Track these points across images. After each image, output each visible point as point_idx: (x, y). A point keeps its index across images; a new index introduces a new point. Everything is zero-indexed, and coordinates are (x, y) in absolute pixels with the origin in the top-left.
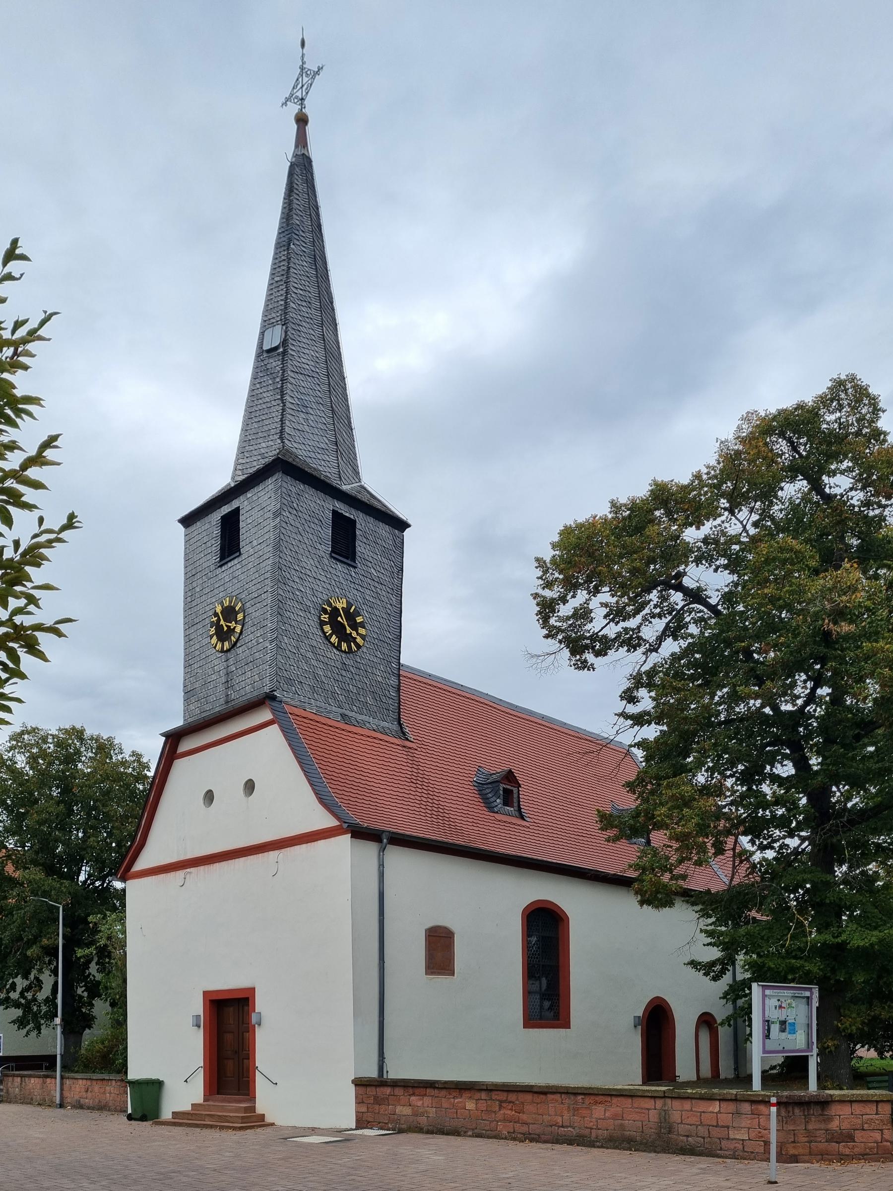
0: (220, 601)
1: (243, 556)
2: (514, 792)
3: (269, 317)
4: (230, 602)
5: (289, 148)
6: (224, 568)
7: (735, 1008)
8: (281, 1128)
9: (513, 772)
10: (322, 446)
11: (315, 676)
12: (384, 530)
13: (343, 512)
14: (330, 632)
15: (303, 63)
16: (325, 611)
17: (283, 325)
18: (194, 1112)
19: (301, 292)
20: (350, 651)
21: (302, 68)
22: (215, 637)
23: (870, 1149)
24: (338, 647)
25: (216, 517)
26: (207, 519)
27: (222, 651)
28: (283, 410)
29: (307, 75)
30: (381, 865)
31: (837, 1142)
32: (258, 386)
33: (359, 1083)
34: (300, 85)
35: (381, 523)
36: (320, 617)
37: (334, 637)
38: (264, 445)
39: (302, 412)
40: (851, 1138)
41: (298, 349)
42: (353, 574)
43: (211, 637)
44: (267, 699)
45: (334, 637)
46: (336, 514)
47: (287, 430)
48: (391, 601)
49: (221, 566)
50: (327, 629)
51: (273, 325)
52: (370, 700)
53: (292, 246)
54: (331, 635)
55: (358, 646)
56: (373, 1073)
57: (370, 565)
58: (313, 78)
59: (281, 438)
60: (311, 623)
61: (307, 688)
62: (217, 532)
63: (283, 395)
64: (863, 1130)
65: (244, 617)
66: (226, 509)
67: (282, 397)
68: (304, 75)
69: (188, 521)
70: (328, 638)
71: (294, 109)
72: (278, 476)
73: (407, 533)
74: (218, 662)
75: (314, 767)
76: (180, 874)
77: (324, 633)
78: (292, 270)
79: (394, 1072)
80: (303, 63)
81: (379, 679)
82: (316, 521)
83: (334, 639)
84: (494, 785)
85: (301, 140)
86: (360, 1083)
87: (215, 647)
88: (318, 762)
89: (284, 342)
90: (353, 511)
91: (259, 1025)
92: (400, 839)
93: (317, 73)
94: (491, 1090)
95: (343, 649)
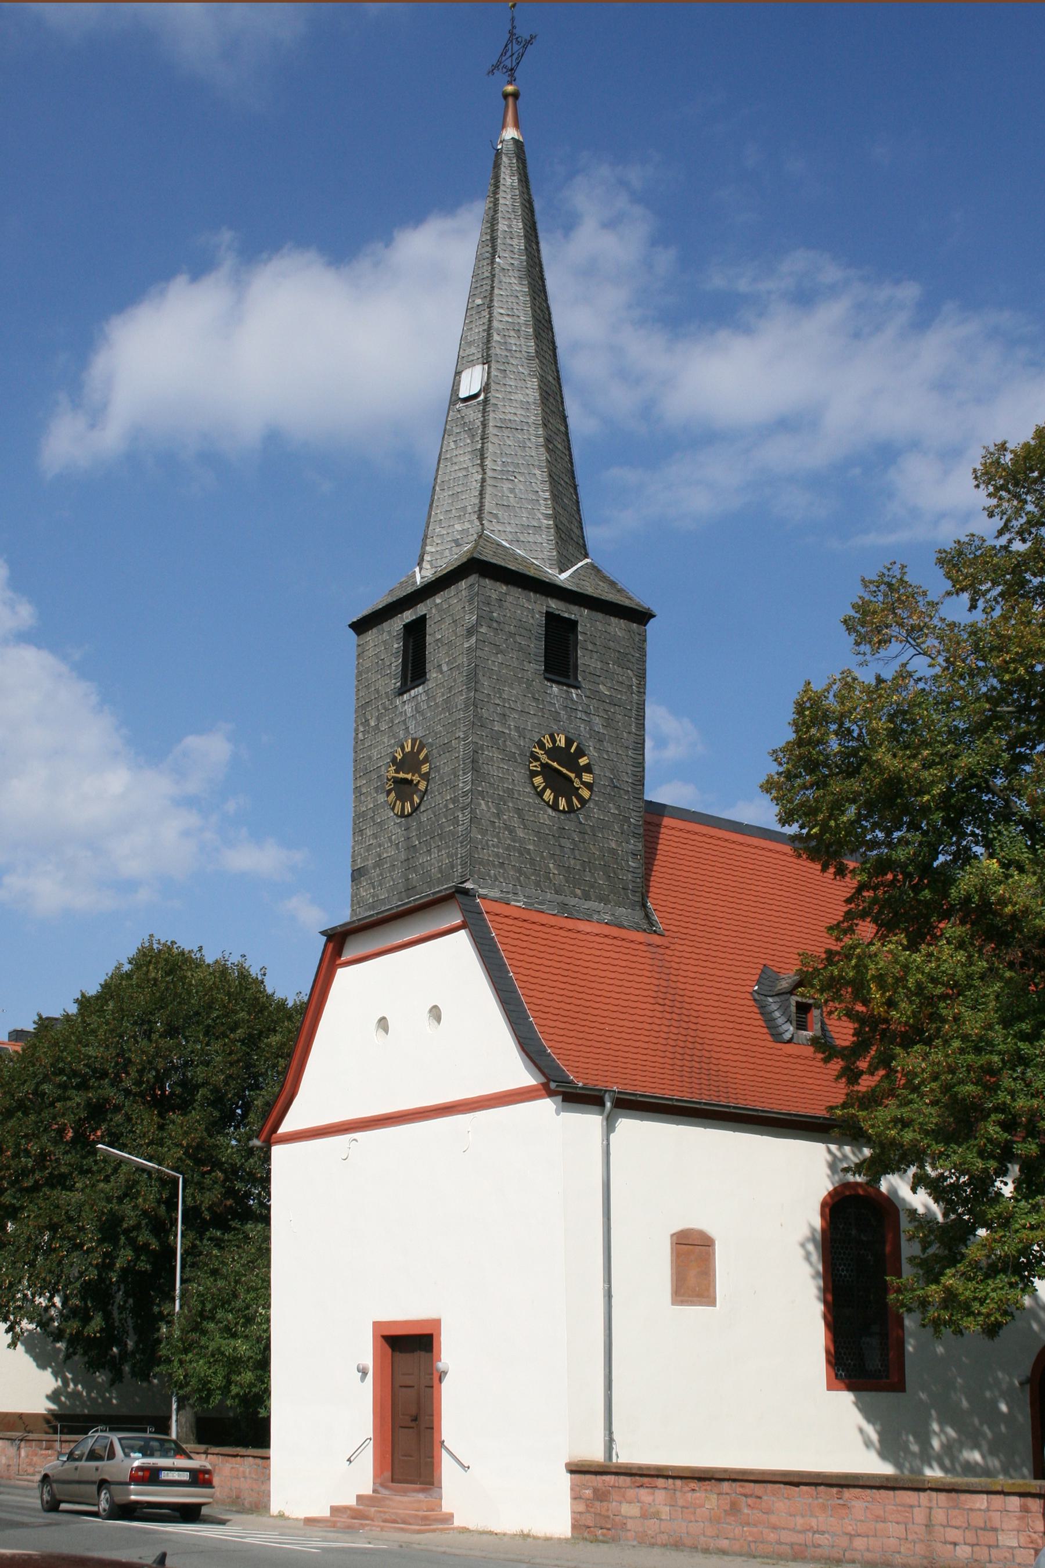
0: (400, 744)
3: (467, 352)
6: (406, 697)
7: (985, 1563)
11: (522, 851)
12: (617, 627)
13: (560, 612)
15: (514, 27)
17: (484, 364)
21: (511, 33)
24: (555, 807)
26: (385, 625)
27: (402, 816)
28: (483, 480)
29: (518, 43)
33: (574, 1468)
34: (509, 54)
35: (612, 618)
37: (548, 791)
44: (459, 895)
45: (548, 791)
46: (550, 616)
51: (472, 364)
53: (498, 260)
54: (544, 790)
55: (583, 801)
56: (596, 1454)
58: (525, 47)
59: (480, 518)
62: (397, 645)
63: (483, 458)
66: (408, 616)
67: (482, 462)
68: (514, 41)
69: (361, 626)
72: (473, 578)
73: (652, 625)
74: (395, 829)
78: (496, 291)
79: (626, 1455)
80: (514, 27)
83: (548, 795)
84: (783, 997)
87: (393, 809)
88: (523, 985)
89: (486, 388)
90: (575, 609)
93: (529, 42)
95: (561, 808)
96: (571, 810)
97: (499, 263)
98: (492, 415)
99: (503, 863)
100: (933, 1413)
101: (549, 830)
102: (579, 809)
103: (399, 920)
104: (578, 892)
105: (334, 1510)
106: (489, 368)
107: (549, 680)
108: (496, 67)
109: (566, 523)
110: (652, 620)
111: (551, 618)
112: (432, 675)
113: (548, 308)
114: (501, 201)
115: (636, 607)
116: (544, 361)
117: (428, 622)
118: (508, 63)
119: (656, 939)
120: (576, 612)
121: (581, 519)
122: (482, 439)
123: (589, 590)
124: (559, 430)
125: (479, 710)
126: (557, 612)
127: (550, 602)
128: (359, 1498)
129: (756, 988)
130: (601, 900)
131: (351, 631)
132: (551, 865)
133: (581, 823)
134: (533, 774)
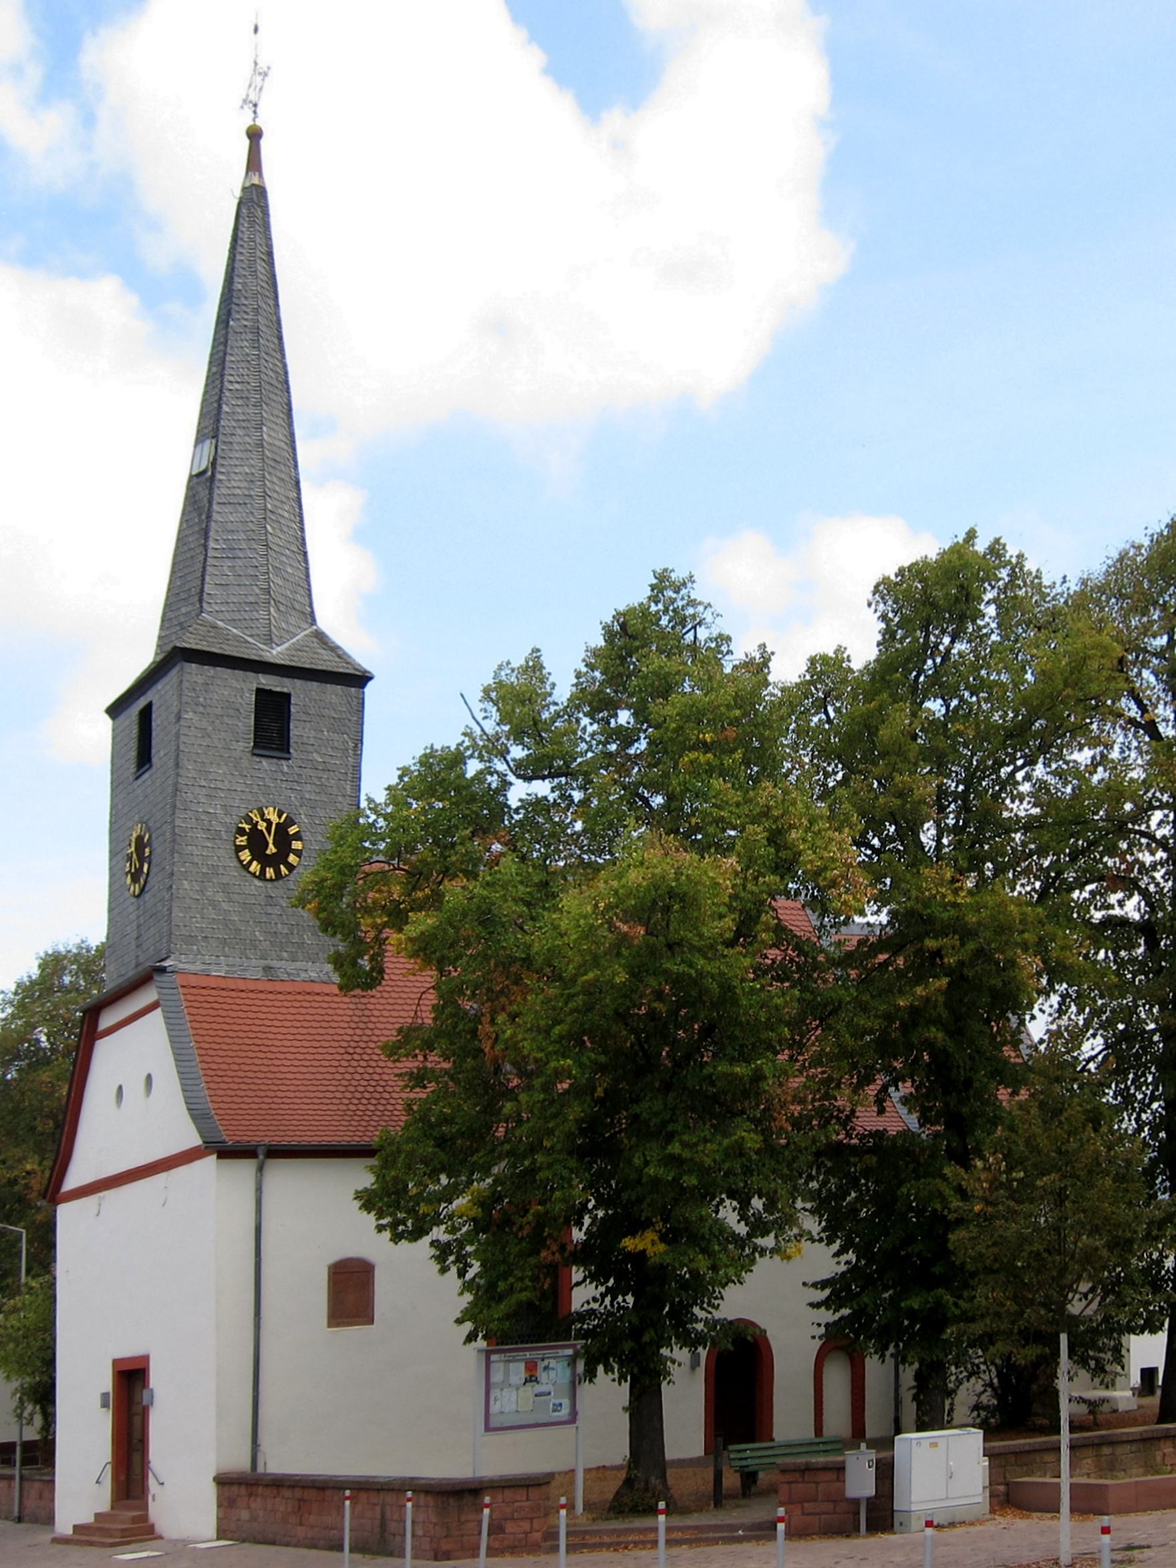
6: (139, 781)
8: (170, 1541)
10: (252, 599)
12: (334, 693)
14: (249, 858)
16: (241, 832)
18: (99, 1525)
19: (237, 386)
24: (262, 876)
27: (134, 896)
30: (259, 1190)
36: (235, 842)
37: (255, 863)
39: (229, 558)
42: (285, 769)
45: (255, 863)
46: (260, 692)
47: (207, 588)
49: (137, 778)
50: (246, 855)
53: (231, 323)
54: (250, 863)
55: (291, 868)
57: (310, 748)
63: (206, 538)
65: (151, 852)
66: (142, 703)
69: (114, 711)
73: (369, 688)
77: (241, 862)
82: (231, 712)
83: (255, 867)
85: (254, 162)
86: (223, 1481)
89: (214, 463)
90: (286, 681)
91: (152, 1404)
92: (283, 1151)
95: (268, 876)
97: (232, 327)
99: (206, 937)
100: (846, 1311)
101: (256, 899)
102: (286, 875)
103: (119, 1002)
106: (217, 441)
111: (262, 695)
115: (352, 671)
116: (274, 426)
117: (154, 708)
126: (268, 688)
128: (97, 1515)
132: (257, 933)
134: (239, 849)
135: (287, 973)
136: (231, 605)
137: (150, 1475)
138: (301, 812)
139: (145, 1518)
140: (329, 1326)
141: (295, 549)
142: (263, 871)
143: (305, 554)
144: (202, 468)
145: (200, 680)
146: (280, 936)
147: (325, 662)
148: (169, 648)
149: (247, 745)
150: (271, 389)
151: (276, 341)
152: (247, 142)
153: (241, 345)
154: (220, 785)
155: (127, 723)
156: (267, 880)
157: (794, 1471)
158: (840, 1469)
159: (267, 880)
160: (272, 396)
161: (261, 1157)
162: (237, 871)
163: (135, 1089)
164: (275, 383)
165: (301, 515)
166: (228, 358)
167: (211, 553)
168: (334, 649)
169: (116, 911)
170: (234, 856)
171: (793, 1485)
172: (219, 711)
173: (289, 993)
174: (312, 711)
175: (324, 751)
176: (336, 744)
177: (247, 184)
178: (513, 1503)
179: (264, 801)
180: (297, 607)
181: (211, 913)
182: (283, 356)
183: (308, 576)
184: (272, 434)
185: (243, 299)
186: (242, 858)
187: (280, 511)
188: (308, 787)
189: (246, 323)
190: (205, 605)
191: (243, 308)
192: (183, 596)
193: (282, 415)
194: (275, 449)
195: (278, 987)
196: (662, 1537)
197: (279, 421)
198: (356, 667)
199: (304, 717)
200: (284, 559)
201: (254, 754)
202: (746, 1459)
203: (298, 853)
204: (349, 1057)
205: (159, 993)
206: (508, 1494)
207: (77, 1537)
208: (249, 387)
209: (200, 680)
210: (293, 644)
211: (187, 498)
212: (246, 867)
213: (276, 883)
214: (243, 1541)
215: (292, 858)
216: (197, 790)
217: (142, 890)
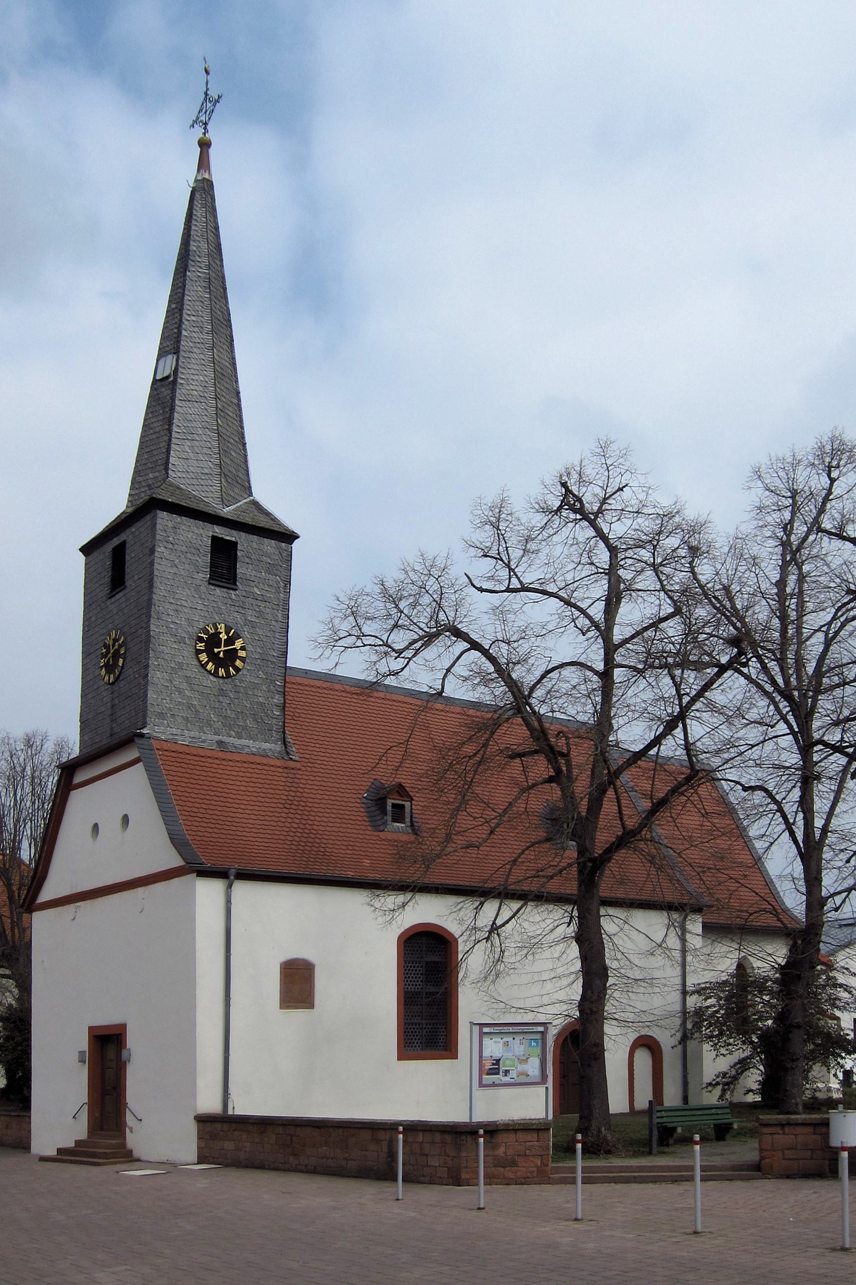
1: (127, 590)
2: (406, 806)
3: (165, 345)
4: (116, 635)
5: (189, 174)
6: (113, 600)
9: (403, 787)
10: (207, 471)
11: (190, 706)
12: (269, 546)
13: (223, 536)
14: (206, 659)
15: (207, 89)
16: (201, 639)
19: (193, 318)
20: (228, 675)
21: (206, 94)
22: (104, 669)
23: (531, 1172)
24: (215, 674)
25: (109, 547)
27: (109, 684)
30: (228, 902)
31: (503, 1167)
32: (150, 416)
36: (196, 647)
38: (151, 476)
40: (513, 1163)
41: (187, 376)
42: (234, 597)
43: (102, 667)
45: (210, 664)
46: (215, 539)
47: (172, 460)
48: (276, 618)
50: (204, 657)
52: (250, 723)
53: (188, 273)
54: (207, 663)
55: (238, 670)
60: (185, 653)
61: (180, 720)
64: (526, 1155)
65: (126, 651)
66: (116, 542)
69: (87, 550)
70: (204, 666)
71: (198, 132)
73: (296, 544)
75: (171, 805)
76: (70, 909)
77: (200, 662)
80: (207, 89)
81: (261, 700)
82: (194, 551)
83: (210, 666)
85: (204, 163)
89: (176, 371)
90: (234, 532)
91: (129, 1061)
93: (217, 101)
94: (285, 1125)
95: (220, 674)
96: (228, 675)
98: (178, 391)
101: (211, 691)
104: (233, 733)
105: (60, 1151)
107: (213, 585)
108: (195, 122)
109: (234, 471)
110: (296, 541)
112: (129, 583)
113: (228, 309)
114: (193, 228)
115: (284, 531)
116: (222, 351)
117: (127, 545)
118: (203, 118)
119: (292, 764)
120: (236, 535)
121: (248, 468)
122: (170, 410)
123: (247, 519)
124: (232, 402)
125: (157, 608)
126: (220, 536)
127: (216, 529)
129: (365, 795)
130: (251, 738)
131: (81, 553)
132: (212, 716)
133: (236, 686)
134: (198, 652)
135: (235, 747)
136: (191, 474)
137: (128, 1112)
138: (245, 629)
139: (124, 1145)
140: (280, 1008)
141: (237, 440)
142: (216, 670)
143: (244, 444)
144: (166, 374)
145: (170, 524)
146: (229, 719)
147: (263, 522)
148: (145, 498)
149: (204, 576)
150: (219, 323)
151: (222, 291)
152: (198, 150)
153: (195, 291)
154: (184, 603)
155: (102, 557)
156: (220, 677)
157: (776, 1125)
158: (826, 1124)
159: (220, 677)
160: (219, 328)
161: (232, 878)
162: (197, 668)
163: (110, 826)
164: (222, 320)
165: (241, 416)
166: (186, 298)
167: (174, 435)
168: (268, 514)
169: (90, 696)
170: (195, 657)
171: (774, 1136)
172: (184, 549)
173: (238, 761)
174: (253, 557)
175: (262, 586)
176: (271, 583)
177: (199, 178)
178: (525, 1142)
179: (217, 618)
180: (239, 481)
181: (177, 697)
182: (227, 302)
183: (246, 461)
184: (220, 355)
185: (197, 257)
186: (201, 659)
187: (227, 411)
188: (250, 612)
189: (199, 274)
190: (170, 472)
191: (198, 264)
192: (150, 465)
193: (226, 342)
194: (222, 366)
195: (229, 756)
196: (579, 1175)
197: (225, 347)
198: (287, 529)
199: (247, 560)
200: (230, 445)
201: (210, 584)
202: (663, 1117)
203: (243, 660)
204: (287, 811)
205: (140, 752)
206: (521, 1136)
207: (59, 1157)
208: (203, 320)
209: (170, 524)
210: (238, 507)
211: (151, 397)
212: (204, 666)
213: (226, 680)
214: (227, 1166)
215: (238, 663)
216: (168, 606)
217: (117, 679)
